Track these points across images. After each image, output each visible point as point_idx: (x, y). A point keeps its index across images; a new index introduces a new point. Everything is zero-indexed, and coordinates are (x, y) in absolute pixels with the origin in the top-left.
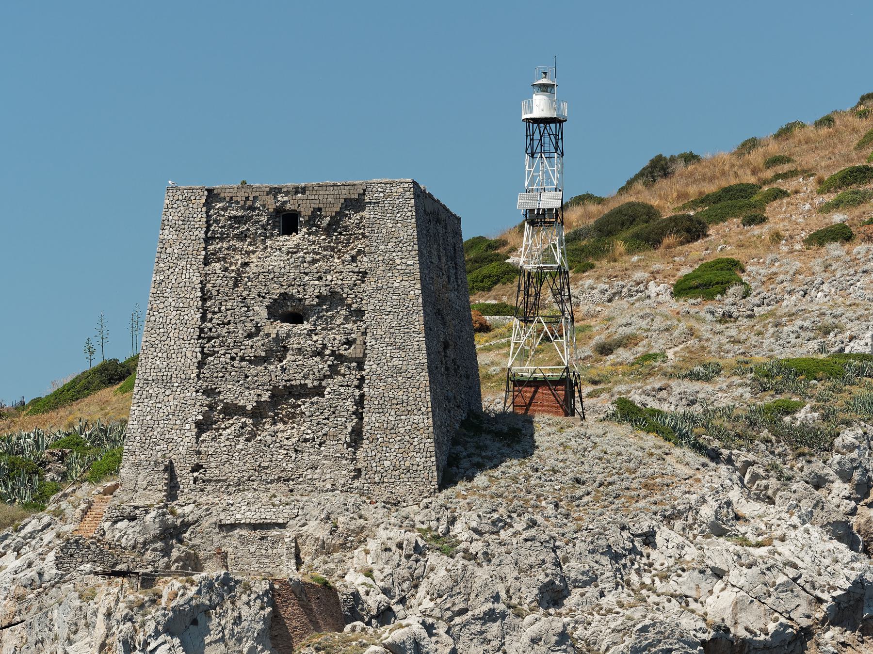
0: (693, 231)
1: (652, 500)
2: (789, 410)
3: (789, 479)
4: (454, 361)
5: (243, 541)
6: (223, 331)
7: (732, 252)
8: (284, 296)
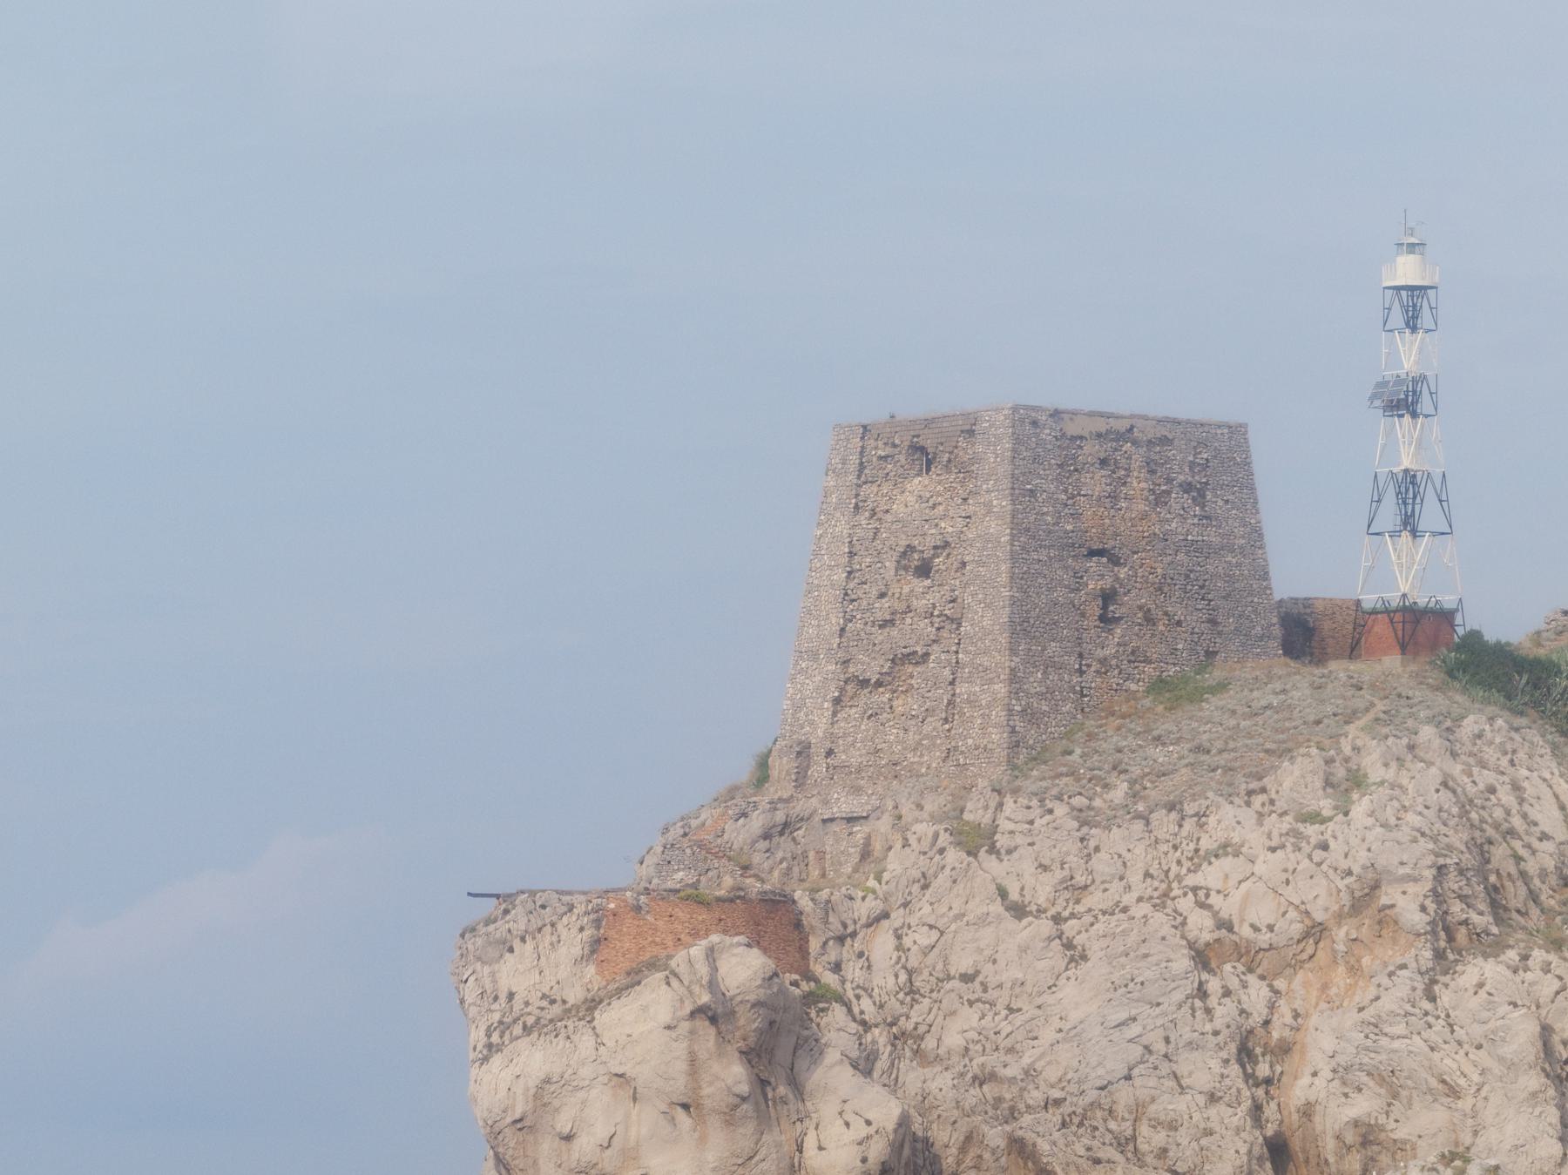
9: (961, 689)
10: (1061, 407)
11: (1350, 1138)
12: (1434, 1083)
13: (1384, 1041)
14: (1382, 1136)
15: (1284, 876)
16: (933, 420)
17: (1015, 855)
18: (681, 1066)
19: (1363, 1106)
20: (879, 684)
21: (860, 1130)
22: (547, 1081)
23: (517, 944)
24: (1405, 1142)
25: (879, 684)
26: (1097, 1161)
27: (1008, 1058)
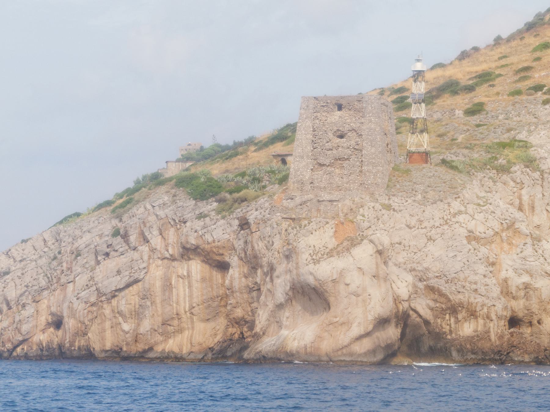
0: (470, 89)
1: (489, 99)
2: (496, 159)
3: (495, 182)
4: (390, 149)
5: (326, 206)
6: (319, 141)
7: (484, 99)
8: (338, 130)
9: (365, 168)
10: (248, 103)
11: (521, 287)
12: (543, 273)
13: (528, 262)
14: (531, 286)
15: (485, 220)
16: (344, 97)
17: (402, 212)
18: (374, 266)
19: (526, 279)
20: (329, 165)
21: (406, 284)
22: (343, 269)
23: (314, 232)
24: (538, 288)
25: (329, 165)
26: (459, 292)
27: (418, 265)
